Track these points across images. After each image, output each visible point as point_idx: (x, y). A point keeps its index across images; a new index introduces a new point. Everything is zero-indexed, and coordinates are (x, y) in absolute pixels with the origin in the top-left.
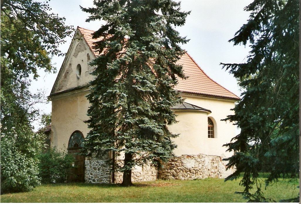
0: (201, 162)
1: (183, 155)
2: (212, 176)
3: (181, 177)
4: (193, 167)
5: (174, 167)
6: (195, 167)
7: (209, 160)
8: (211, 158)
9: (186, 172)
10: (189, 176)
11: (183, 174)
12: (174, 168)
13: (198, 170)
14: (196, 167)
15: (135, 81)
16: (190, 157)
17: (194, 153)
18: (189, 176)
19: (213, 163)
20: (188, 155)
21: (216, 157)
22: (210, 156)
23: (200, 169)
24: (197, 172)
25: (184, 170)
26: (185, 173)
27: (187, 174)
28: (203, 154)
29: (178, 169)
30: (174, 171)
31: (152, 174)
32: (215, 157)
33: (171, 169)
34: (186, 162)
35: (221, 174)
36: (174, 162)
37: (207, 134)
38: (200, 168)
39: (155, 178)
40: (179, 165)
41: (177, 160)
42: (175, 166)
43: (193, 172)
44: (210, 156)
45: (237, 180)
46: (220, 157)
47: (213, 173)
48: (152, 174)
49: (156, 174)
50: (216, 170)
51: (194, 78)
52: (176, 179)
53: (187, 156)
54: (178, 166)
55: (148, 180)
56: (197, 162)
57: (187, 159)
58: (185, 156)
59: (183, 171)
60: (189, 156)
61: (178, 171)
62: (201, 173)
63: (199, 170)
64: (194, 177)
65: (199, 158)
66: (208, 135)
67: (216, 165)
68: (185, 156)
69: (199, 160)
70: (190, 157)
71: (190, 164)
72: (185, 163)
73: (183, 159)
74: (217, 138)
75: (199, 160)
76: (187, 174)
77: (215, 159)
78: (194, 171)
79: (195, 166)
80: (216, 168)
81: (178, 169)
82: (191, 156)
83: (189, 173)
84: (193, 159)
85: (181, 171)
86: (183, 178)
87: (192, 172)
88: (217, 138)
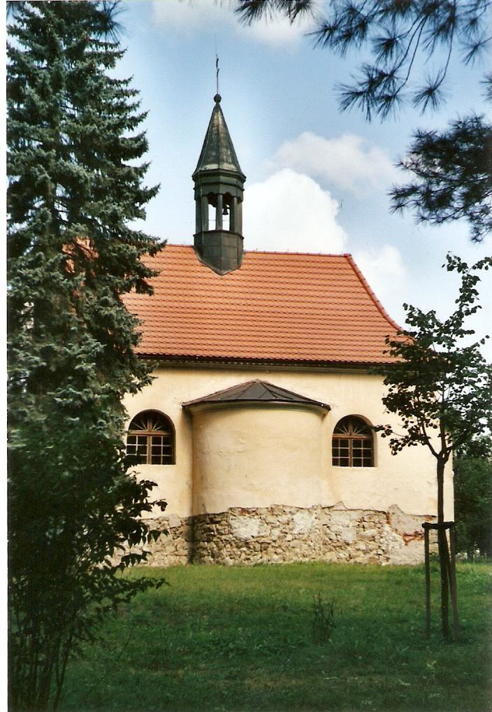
0: (278, 523)
1: (231, 509)
2: (358, 560)
3: (228, 558)
4: (255, 534)
5: (214, 536)
6: (259, 537)
7: (351, 520)
8: (356, 516)
9: (238, 547)
10: (243, 556)
11: (232, 553)
12: (215, 540)
13: (269, 544)
14: (263, 537)
15: (423, 333)
16: (249, 513)
17: (261, 503)
18: (243, 556)
19: (364, 527)
20: (243, 507)
21: (373, 513)
22: (351, 510)
23: (275, 541)
24: (264, 547)
25: (232, 543)
26: (235, 549)
27: (239, 553)
28: (283, 506)
29: (222, 541)
30: (215, 546)
31: (176, 553)
32: (368, 513)
33: (209, 541)
34: (238, 524)
35: (387, 555)
36: (214, 526)
37: (329, 456)
38: (274, 538)
39: (184, 560)
40: (223, 532)
41: (220, 519)
42: (216, 533)
43: (254, 547)
44: (351, 510)
45: (125, 571)
46: (384, 513)
47: (360, 553)
48: (176, 553)
49: (186, 552)
50: (372, 545)
51: (321, 306)
52: (218, 562)
53: (240, 510)
54: (222, 534)
55: (162, 564)
56: (267, 524)
57: (241, 518)
58: (237, 512)
59: (231, 545)
60: (244, 511)
61: (221, 544)
62: (279, 550)
63: (273, 544)
64: (257, 558)
65: (273, 515)
66: (333, 459)
67: (369, 532)
68: (237, 512)
69: (271, 519)
70: (249, 513)
71: (247, 529)
72: (236, 526)
73: (231, 517)
74: (377, 466)
75: (271, 519)
76: (239, 553)
77: (370, 518)
78: (258, 546)
79: (259, 533)
80: (374, 540)
81: (222, 541)
82: (250, 510)
83: (245, 549)
84: (256, 517)
85: (229, 545)
86: (231, 562)
87: (252, 547)
88: (377, 466)
